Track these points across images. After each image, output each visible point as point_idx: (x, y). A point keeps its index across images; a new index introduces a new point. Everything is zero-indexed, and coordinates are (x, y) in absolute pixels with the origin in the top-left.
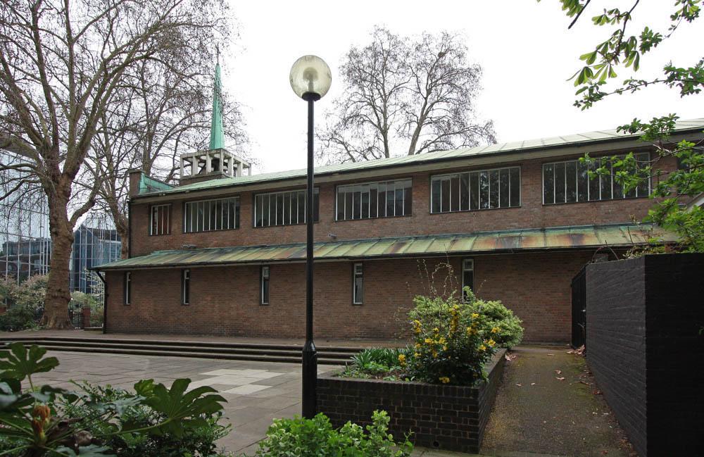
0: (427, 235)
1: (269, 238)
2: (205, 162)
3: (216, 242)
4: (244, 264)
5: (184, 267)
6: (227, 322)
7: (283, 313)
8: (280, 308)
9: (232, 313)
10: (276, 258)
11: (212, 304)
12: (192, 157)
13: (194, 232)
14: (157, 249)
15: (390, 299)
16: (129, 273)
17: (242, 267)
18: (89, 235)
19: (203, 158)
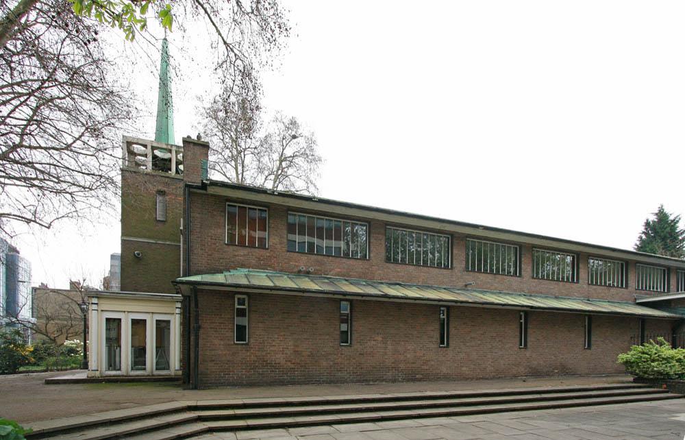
1: (403, 276)
3: (339, 270)
4: (480, 306)
5: (341, 297)
6: (402, 366)
7: (462, 355)
8: (459, 350)
9: (409, 356)
11: (384, 346)
13: (618, 286)
15: (545, 344)
17: (651, 319)
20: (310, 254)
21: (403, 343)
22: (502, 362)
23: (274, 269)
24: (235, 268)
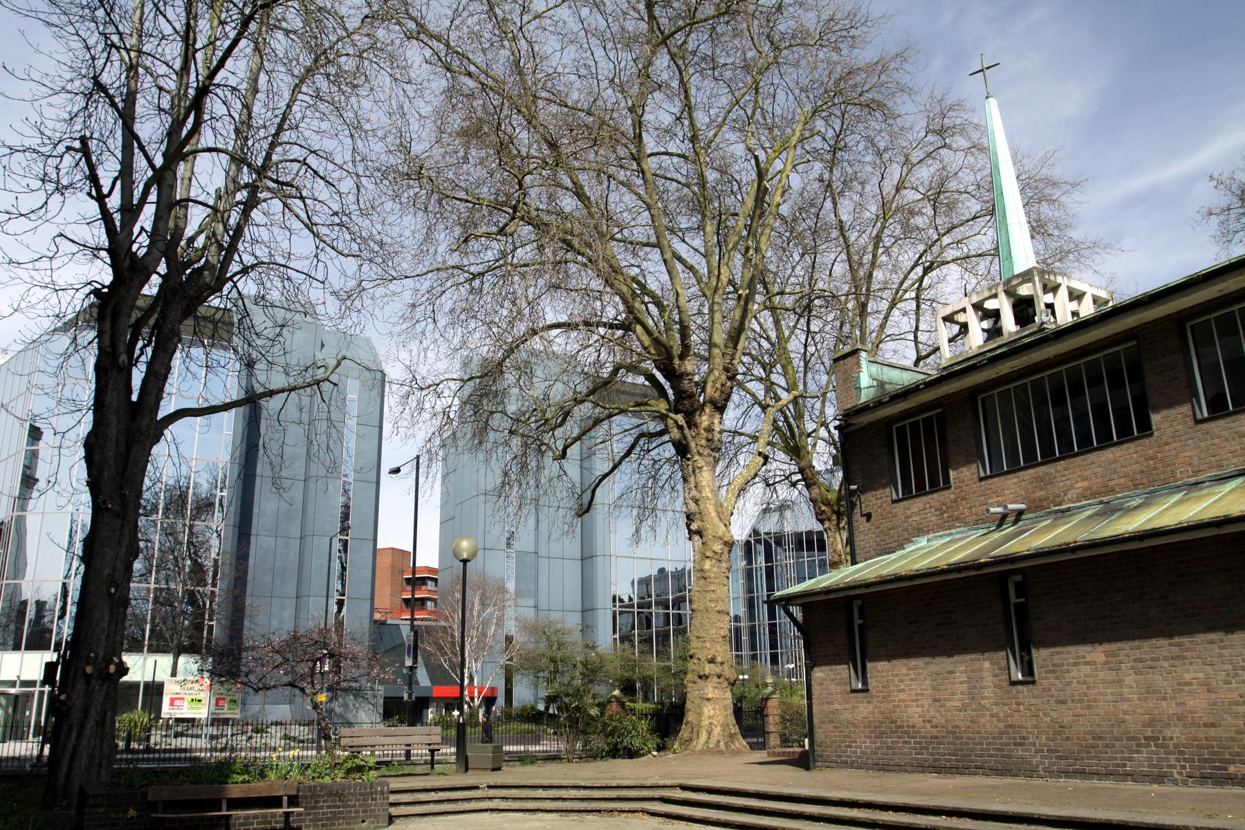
3: (1085, 484)
12: (964, 310)
14: (920, 532)
16: (859, 602)
21: (1165, 664)
23: (966, 524)
24: (909, 541)
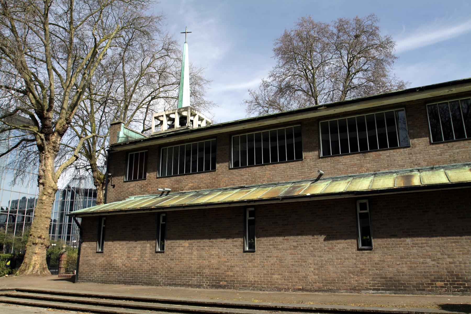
0: (432, 166)
1: (247, 178)
2: (173, 120)
3: (192, 184)
6: (207, 271)
8: (268, 255)
10: (265, 197)
12: (163, 116)
18: (73, 193)
19: (172, 116)
20: (274, 164)
21: (207, 248)
22: (331, 268)
